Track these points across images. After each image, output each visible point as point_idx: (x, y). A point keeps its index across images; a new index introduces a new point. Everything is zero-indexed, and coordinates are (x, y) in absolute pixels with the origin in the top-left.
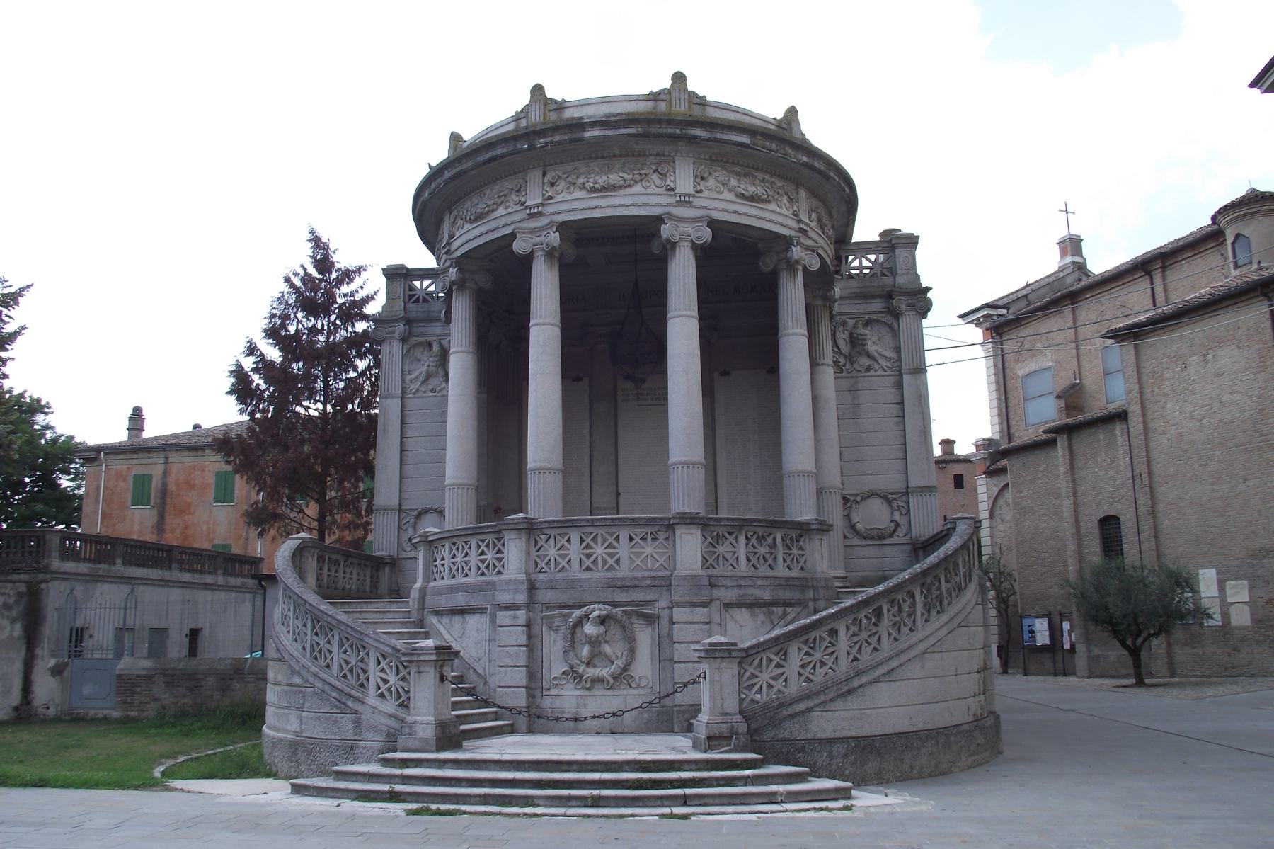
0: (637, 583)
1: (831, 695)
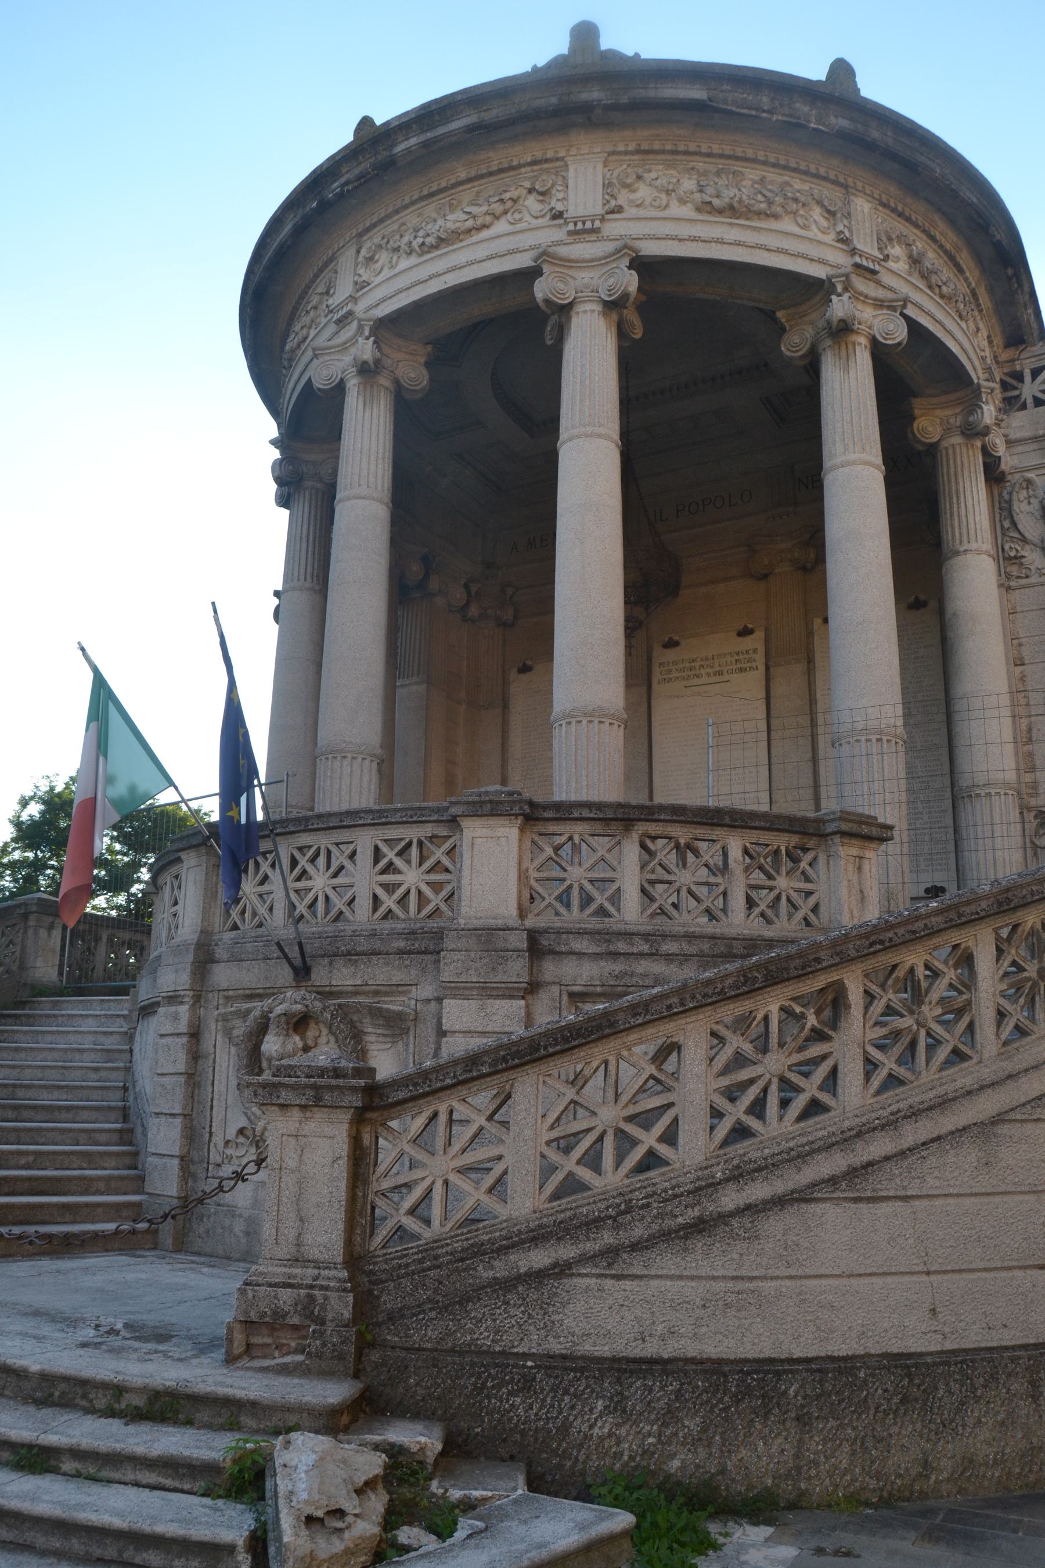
0: (377, 945)
1: (639, 1232)
